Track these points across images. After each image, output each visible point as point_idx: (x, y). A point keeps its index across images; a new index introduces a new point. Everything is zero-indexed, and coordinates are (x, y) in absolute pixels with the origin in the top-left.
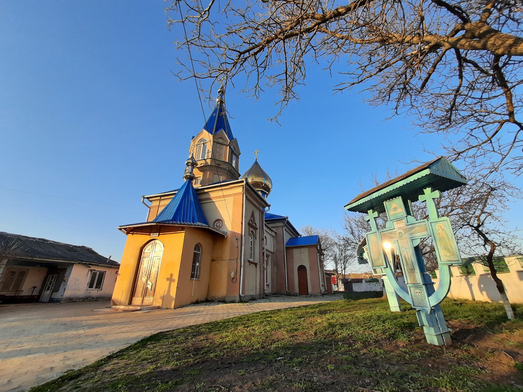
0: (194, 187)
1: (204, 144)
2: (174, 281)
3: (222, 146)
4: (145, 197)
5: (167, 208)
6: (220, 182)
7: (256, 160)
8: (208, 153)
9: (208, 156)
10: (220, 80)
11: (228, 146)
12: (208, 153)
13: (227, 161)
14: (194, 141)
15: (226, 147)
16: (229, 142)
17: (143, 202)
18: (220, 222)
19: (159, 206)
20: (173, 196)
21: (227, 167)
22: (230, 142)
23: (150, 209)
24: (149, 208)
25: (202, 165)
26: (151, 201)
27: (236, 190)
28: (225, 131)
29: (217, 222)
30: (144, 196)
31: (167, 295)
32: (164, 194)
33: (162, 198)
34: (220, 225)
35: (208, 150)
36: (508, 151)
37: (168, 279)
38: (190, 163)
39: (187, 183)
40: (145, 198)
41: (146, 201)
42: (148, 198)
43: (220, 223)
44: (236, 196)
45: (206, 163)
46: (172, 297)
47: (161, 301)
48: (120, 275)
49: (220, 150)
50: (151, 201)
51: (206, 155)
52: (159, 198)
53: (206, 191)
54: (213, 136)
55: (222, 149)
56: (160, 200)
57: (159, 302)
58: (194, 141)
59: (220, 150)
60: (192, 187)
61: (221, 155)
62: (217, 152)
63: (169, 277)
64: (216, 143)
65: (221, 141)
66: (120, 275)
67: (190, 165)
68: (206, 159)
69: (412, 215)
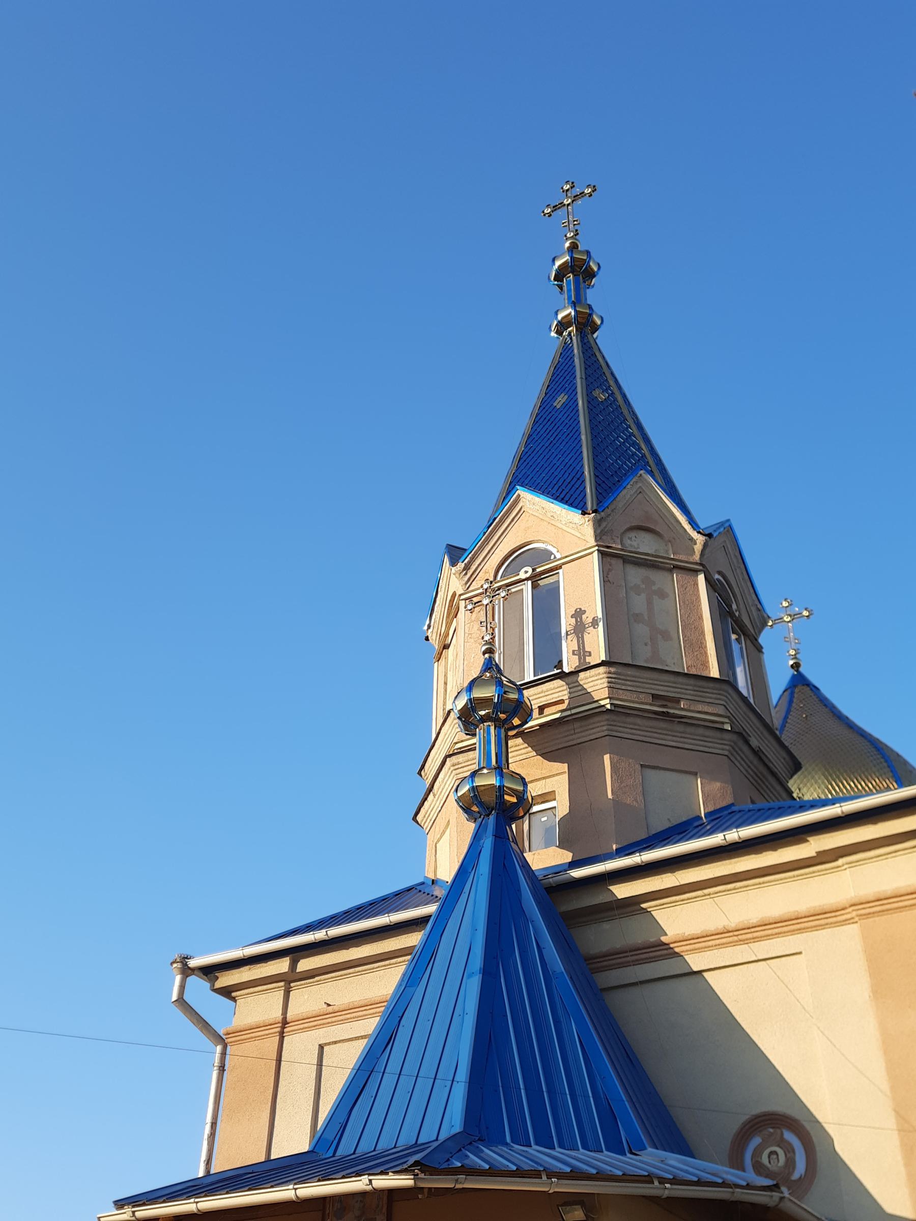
0: (534, 867)
1: (535, 579)
3: (658, 577)
4: (193, 963)
5: (391, 1039)
7: (796, 666)
8: (579, 629)
9: (582, 652)
10: (555, 208)
11: (696, 572)
12: (579, 629)
13: (715, 673)
14: (467, 568)
15: (687, 577)
16: (698, 548)
17: (181, 1002)
18: (788, 1136)
19: (285, 1022)
20: (414, 939)
21: (721, 710)
22: (705, 545)
23: (224, 1054)
24: (219, 1039)
25: (552, 715)
26: (227, 992)
28: (651, 473)
29: (756, 1141)
30: (184, 960)
32: (320, 935)
33: (305, 965)
34: (790, 1163)
35: (578, 614)
38: (484, 702)
39: (488, 843)
40: (193, 970)
41: (198, 986)
42: (209, 971)
43: (789, 1150)
45: (579, 695)
49: (650, 603)
50: (227, 992)
51: (567, 648)
52: (282, 966)
53: (622, 891)
54: (597, 524)
55: (663, 595)
56: (289, 980)
58: (467, 568)
59: (650, 603)
60: (526, 865)
61: (666, 636)
62: (637, 617)
64: (620, 562)
65: (644, 545)
67: (483, 719)
68: (575, 673)
69: (567, 1148)
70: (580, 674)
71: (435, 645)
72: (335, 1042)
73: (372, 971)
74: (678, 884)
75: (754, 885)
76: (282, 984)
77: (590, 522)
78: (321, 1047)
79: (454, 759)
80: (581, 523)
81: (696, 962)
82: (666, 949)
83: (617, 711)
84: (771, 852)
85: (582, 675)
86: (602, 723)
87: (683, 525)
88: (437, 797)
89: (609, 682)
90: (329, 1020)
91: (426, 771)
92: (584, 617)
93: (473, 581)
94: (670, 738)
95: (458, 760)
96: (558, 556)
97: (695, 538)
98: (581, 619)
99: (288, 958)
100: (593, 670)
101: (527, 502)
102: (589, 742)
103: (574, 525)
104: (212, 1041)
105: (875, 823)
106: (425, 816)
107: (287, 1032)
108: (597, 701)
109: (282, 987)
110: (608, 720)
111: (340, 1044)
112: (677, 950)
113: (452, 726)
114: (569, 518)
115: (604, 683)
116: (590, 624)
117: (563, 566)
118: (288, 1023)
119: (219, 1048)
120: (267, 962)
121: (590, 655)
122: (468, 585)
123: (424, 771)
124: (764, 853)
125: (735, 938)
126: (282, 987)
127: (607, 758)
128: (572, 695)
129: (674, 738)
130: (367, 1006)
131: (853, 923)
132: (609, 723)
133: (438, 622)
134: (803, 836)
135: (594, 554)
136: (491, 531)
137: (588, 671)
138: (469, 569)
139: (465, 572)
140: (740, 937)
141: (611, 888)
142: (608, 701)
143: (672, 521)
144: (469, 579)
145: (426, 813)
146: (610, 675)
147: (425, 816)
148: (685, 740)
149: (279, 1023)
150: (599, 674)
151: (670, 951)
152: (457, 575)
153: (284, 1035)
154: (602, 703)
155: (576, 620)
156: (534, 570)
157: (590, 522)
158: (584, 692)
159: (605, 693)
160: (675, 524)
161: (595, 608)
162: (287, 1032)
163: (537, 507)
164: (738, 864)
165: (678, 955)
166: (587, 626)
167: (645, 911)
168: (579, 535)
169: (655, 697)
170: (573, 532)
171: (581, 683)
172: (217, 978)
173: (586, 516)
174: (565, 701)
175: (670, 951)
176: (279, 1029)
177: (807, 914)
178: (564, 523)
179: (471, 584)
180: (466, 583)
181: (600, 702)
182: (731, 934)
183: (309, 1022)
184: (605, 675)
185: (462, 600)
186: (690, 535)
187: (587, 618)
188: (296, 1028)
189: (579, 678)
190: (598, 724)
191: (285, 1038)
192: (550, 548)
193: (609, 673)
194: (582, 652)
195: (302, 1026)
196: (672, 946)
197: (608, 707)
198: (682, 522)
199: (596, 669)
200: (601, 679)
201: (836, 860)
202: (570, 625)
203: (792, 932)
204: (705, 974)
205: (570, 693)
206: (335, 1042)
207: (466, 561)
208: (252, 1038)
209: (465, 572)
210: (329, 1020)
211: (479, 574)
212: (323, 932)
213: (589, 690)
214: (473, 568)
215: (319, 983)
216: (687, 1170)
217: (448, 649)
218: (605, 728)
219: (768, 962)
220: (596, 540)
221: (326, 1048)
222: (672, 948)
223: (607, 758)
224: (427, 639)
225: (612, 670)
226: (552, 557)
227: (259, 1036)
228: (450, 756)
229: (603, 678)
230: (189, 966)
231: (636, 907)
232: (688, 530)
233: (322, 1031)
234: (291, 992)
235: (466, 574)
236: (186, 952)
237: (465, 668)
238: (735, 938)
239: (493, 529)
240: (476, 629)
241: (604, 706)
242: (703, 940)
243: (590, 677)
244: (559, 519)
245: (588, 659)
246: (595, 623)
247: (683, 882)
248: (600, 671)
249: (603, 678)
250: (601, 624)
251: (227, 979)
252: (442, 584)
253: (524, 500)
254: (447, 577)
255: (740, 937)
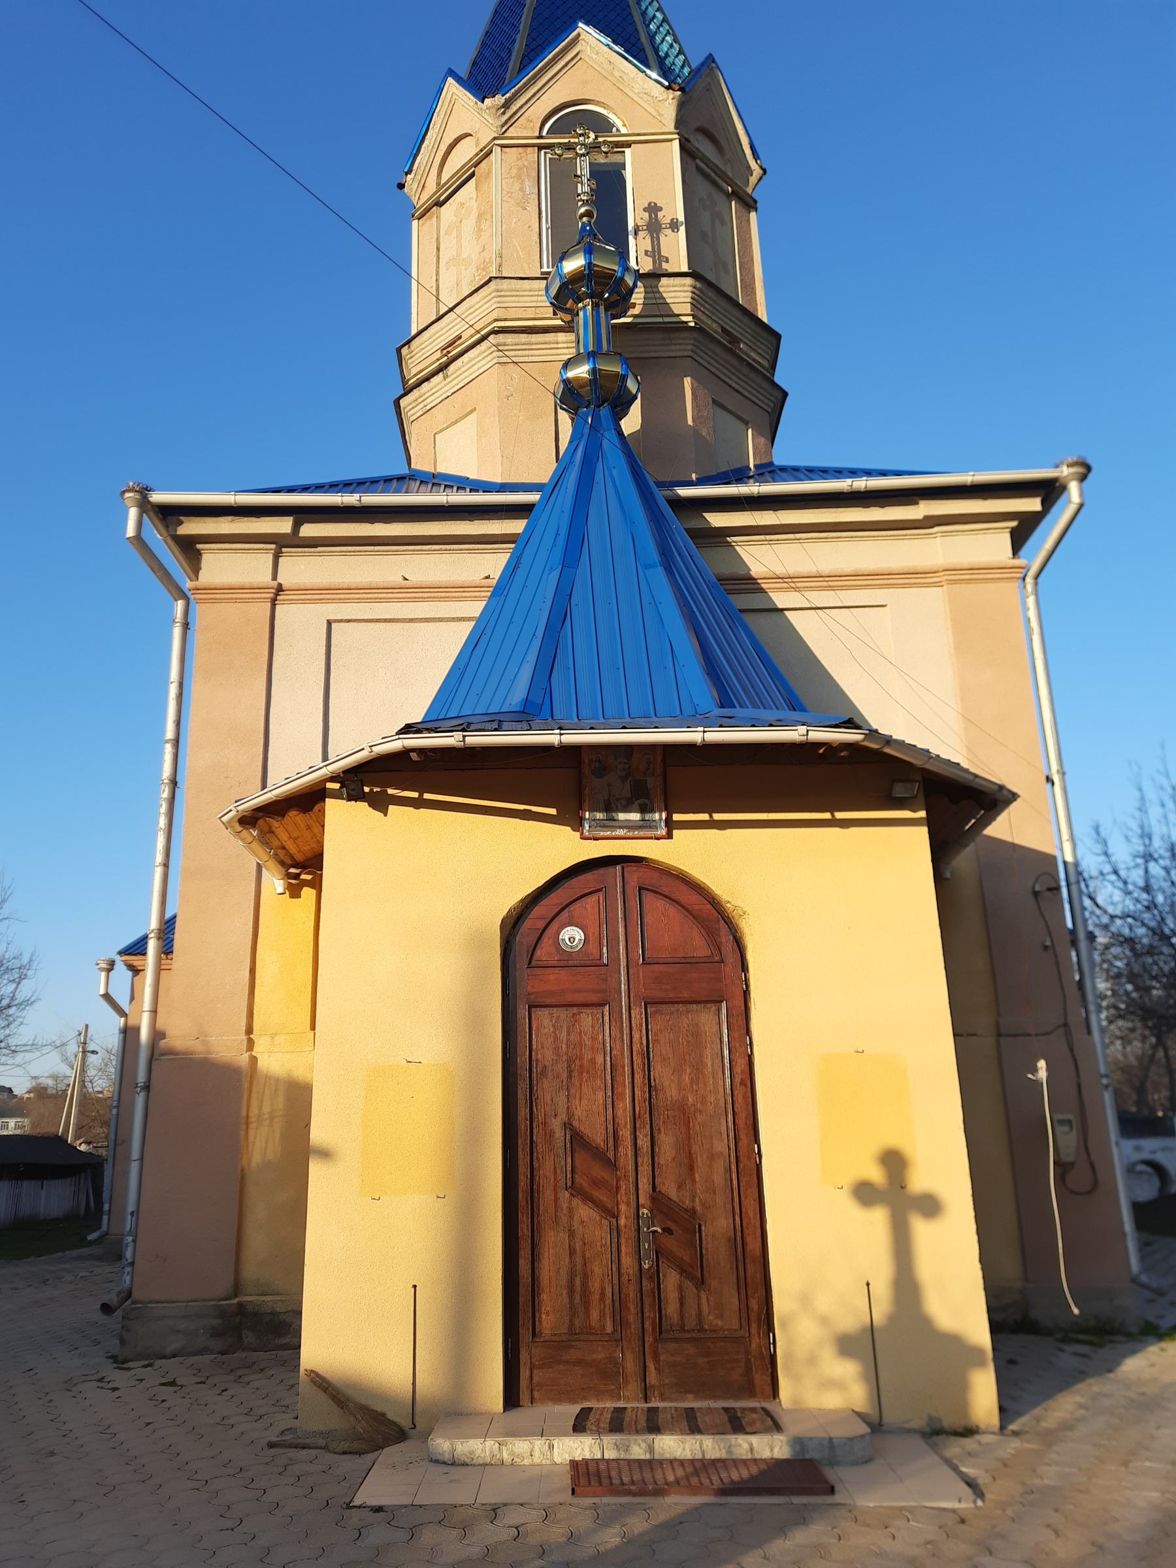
2: (930, 1206)
6: (740, 475)
8: (654, 228)
9: (655, 253)
12: (654, 228)
14: (507, 105)
20: (517, 526)
27: (325, 561)
30: (144, 491)
31: (892, 1319)
33: (309, 530)
35: (653, 209)
36: (805, 594)
37: (864, 1193)
42: (170, 514)
44: (953, 586)
46: (954, 1343)
47: (847, 1371)
48: (325, 1154)
52: (284, 525)
53: (717, 520)
56: (292, 542)
57: (830, 1384)
58: (507, 105)
63: (876, 1174)
66: (325, 1154)
70: (662, 279)
71: (413, 198)
72: (349, 621)
73: (396, 553)
74: (778, 523)
75: (845, 538)
76: (273, 546)
77: (675, 100)
78: (329, 623)
79: (501, 338)
80: (661, 99)
81: (780, 599)
82: (754, 584)
83: (698, 329)
84: (878, 508)
85: (664, 281)
86: (687, 341)
87: (744, 147)
88: (448, 380)
89: (692, 298)
90: (342, 596)
91: (412, 348)
92: (660, 214)
93: (511, 125)
94: (735, 378)
95: (506, 341)
96: (624, 130)
97: (753, 168)
98: (656, 216)
99: (291, 519)
100: (679, 278)
101: (588, 47)
102: (667, 359)
103: (649, 98)
104: (174, 593)
105: (985, 499)
106: (417, 400)
107: (281, 600)
108: (679, 315)
109: (271, 550)
110: (695, 339)
111: (353, 624)
112: (763, 586)
113: (489, 297)
114: (645, 86)
115: (687, 297)
116: (668, 226)
117: (633, 145)
118: (284, 591)
119: (180, 604)
120: (259, 517)
121: (667, 261)
122: (504, 129)
123: (409, 347)
124: (872, 508)
125: (825, 584)
126: (271, 550)
127: (687, 381)
128: (648, 301)
129: (738, 381)
130: (395, 588)
131: (939, 586)
132: (695, 343)
133: (422, 168)
134: (915, 498)
135: (673, 142)
136: (540, 68)
137: (672, 278)
138: (508, 108)
139: (503, 110)
140: (830, 583)
141: (705, 515)
142: (690, 318)
143: (735, 140)
144: (506, 122)
145: (420, 397)
146: (694, 290)
147: (417, 400)
148: (746, 386)
149: (272, 588)
150: (684, 285)
151: (755, 586)
152: (493, 111)
153: (276, 602)
154: (684, 319)
155: (650, 216)
156: (596, 137)
157: (675, 100)
158: (662, 301)
159: (687, 309)
160: (735, 142)
161: (676, 208)
162: (281, 600)
163: (602, 59)
164: (843, 514)
165: (762, 591)
166: (645, 228)
167: (729, 545)
168: (654, 113)
169: (724, 329)
170: (646, 106)
171: (661, 290)
172: (181, 523)
173: (670, 91)
174: (637, 306)
175: (755, 586)
176: (271, 595)
177: (901, 572)
178: (637, 91)
179: (508, 129)
180: (503, 126)
181: (681, 317)
182: (822, 579)
183: (332, 594)
184: (690, 289)
185: (497, 145)
186: (748, 163)
187: (665, 217)
188: (291, 597)
189: (660, 284)
190: (681, 341)
191: (277, 606)
192: (613, 118)
193: (695, 287)
194: (655, 253)
195: (303, 597)
196: (759, 581)
197: (692, 324)
198: (743, 144)
199: (682, 278)
200: (685, 291)
201: (932, 527)
202: (642, 218)
203: (881, 586)
204: (786, 613)
205: (645, 298)
206: (349, 621)
207: (508, 95)
208: (232, 599)
209: (503, 110)
210: (342, 596)
211: (520, 119)
212: (356, 496)
213: (669, 301)
214: (514, 108)
215: (320, 554)
216: (926, 518)
217: (441, 207)
218: (689, 347)
219: (851, 609)
220: (676, 128)
221: (334, 626)
222: (759, 584)
223: (687, 381)
224: (401, 186)
225: (698, 285)
226: (614, 129)
227: (242, 599)
228: (495, 332)
229: (687, 291)
230: (150, 499)
231: (721, 540)
232: (748, 156)
233: (331, 607)
234: (280, 559)
235: (504, 113)
236: (151, 485)
237: (504, 234)
238: (825, 584)
239: (543, 66)
240: (518, 189)
241: (686, 322)
242: (789, 581)
243: (673, 286)
244: (630, 83)
245: (664, 265)
246: (674, 226)
247: (783, 522)
248: (685, 282)
249: (687, 291)
250: (683, 229)
251: (191, 527)
252: (437, 120)
253: (583, 42)
254: (446, 112)
255: (830, 583)
